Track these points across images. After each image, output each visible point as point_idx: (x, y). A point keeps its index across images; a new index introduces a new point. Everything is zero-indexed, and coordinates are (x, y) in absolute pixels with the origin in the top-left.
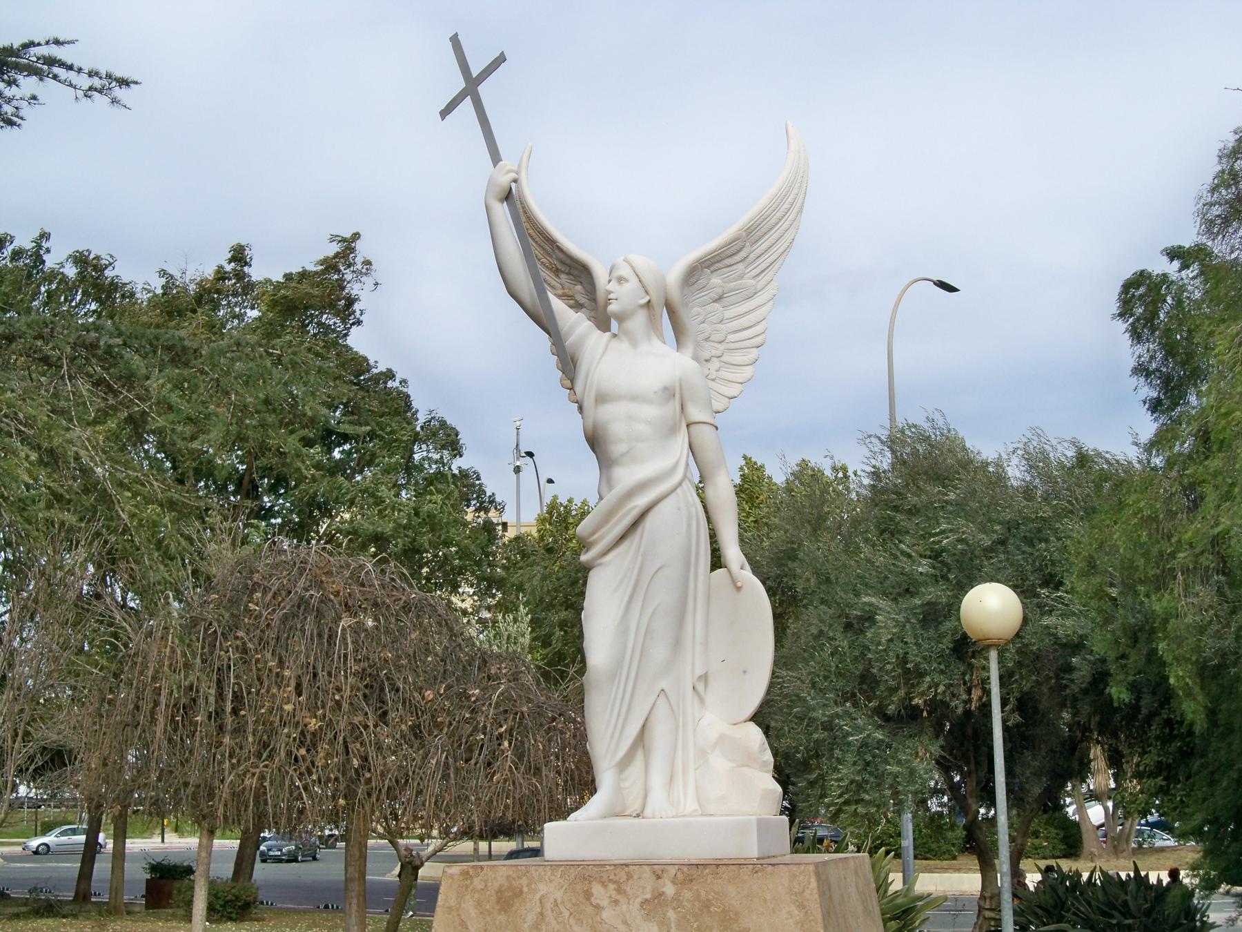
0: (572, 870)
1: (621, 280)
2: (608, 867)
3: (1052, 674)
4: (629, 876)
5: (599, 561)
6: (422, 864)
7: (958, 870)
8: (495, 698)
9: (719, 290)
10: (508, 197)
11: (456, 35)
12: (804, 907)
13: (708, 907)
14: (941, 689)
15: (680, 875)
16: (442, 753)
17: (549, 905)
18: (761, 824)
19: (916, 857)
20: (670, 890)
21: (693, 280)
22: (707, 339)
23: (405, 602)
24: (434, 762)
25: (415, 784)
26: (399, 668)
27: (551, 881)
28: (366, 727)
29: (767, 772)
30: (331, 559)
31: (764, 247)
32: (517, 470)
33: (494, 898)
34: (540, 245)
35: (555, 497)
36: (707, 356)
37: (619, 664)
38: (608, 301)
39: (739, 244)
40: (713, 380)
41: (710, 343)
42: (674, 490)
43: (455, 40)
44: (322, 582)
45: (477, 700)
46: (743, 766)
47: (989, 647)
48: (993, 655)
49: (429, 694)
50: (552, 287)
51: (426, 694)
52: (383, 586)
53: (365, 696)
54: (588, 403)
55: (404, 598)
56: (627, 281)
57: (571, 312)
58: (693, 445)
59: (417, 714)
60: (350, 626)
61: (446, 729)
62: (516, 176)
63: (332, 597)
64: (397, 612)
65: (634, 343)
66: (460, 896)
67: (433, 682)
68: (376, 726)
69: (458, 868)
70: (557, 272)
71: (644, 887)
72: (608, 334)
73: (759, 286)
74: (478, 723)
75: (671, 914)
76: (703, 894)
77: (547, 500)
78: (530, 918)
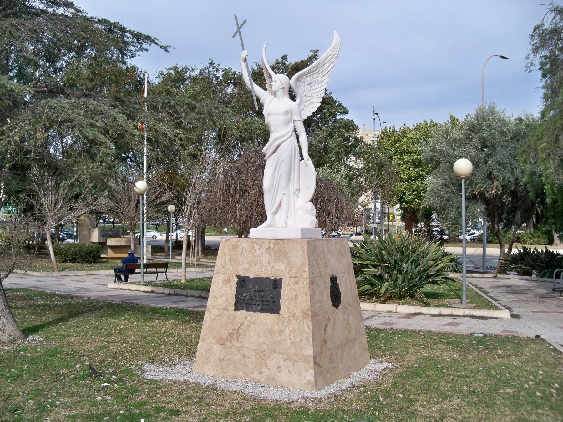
3: (522, 185)
9: (309, 82)
14: (483, 189)
15: (275, 243)
17: (244, 249)
20: (272, 246)
32: (374, 119)
35: (386, 127)
36: (305, 101)
43: (236, 16)
47: (463, 178)
48: (463, 181)
65: (279, 99)
66: (224, 247)
73: (323, 80)
75: (272, 252)
77: (383, 128)
78: (240, 252)
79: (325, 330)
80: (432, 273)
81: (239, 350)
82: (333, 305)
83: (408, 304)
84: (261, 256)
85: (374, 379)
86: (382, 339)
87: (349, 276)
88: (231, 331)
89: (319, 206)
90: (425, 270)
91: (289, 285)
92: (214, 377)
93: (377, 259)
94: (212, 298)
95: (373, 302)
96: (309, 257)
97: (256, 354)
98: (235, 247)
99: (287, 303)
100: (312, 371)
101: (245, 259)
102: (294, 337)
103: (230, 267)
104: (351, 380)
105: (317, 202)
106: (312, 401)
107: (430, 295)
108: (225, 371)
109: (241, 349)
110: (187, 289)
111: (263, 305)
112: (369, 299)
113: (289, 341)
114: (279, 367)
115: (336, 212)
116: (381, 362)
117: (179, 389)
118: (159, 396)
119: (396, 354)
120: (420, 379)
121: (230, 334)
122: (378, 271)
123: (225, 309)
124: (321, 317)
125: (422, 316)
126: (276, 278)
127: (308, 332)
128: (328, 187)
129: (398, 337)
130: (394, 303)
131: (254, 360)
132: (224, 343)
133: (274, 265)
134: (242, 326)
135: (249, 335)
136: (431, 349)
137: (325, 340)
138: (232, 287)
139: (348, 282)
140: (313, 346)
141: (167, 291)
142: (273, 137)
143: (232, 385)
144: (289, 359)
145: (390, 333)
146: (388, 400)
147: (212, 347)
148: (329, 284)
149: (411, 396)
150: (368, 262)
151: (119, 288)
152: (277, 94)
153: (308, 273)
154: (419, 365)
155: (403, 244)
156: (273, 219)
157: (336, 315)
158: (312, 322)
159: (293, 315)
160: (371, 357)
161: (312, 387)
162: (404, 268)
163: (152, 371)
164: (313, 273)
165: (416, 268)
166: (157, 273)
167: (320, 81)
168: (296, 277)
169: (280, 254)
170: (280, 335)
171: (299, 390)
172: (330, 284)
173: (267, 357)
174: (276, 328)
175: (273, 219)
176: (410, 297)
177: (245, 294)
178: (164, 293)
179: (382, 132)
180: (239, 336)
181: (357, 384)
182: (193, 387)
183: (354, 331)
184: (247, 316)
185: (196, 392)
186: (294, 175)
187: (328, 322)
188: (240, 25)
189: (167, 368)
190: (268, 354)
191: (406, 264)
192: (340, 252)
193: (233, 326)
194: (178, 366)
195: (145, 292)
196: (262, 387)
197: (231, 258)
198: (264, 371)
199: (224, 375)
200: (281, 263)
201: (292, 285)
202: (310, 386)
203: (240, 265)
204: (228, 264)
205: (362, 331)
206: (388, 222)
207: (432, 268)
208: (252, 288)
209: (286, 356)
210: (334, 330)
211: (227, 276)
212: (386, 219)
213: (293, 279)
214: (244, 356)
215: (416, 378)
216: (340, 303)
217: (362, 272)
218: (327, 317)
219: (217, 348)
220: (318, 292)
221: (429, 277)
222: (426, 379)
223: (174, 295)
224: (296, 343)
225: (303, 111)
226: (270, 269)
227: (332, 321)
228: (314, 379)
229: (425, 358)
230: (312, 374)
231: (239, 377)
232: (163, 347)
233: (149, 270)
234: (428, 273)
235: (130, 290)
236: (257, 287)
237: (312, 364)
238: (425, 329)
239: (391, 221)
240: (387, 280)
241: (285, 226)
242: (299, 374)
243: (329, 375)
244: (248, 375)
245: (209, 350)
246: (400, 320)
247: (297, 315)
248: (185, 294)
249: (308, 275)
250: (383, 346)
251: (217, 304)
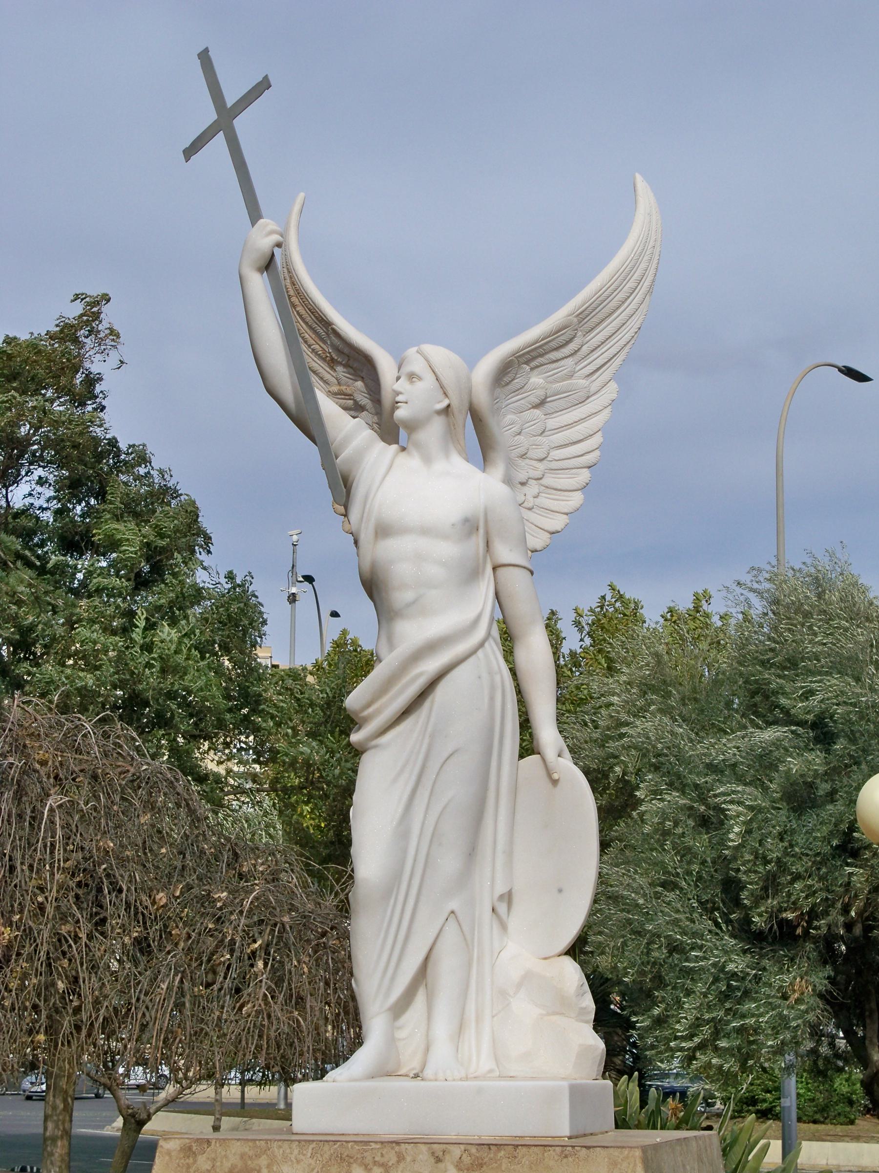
0: (326, 1148)
1: (412, 377)
2: (373, 1146)
4: (401, 1158)
5: (374, 743)
6: (149, 1118)
7: (857, 1138)
8: (247, 904)
9: (541, 393)
10: (268, 265)
11: (206, 50)
15: (467, 1159)
16: (176, 975)
18: (577, 1094)
19: (799, 1120)
21: (506, 379)
22: (523, 456)
23: (133, 775)
24: (164, 986)
25: (140, 1015)
26: (123, 862)
27: (298, 1162)
28: (76, 939)
29: (587, 1022)
30: (39, 717)
31: (600, 338)
32: (293, 598)
34: (310, 327)
36: (522, 476)
38: (395, 405)
39: (567, 334)
40: (530, 509)
41: (527, 461)
42: (473, 652)
44: (25, 746)
45: (225, 905)
46: (555, 1013)
49: (162, 897)
50: (326, 382)
51: (158, 897)
52: (106, 755)
53: (77, 897)
54: (366, 536)
55: (132, 770)
56: (420, 379)
57: (345, 417)
58: (501, 594)
59: (145, 923)
60: (60, 806)
61: (182, 944)
63: (37, 766)
64: (123, 789)
65: (427, 460)
67: (167, 880)
68: (90, 937)
69: (177, 1141)
70: (332, 363)
72: (394, 447)
73: (593, 388)
74: (224, 936)
167: (582, 394)
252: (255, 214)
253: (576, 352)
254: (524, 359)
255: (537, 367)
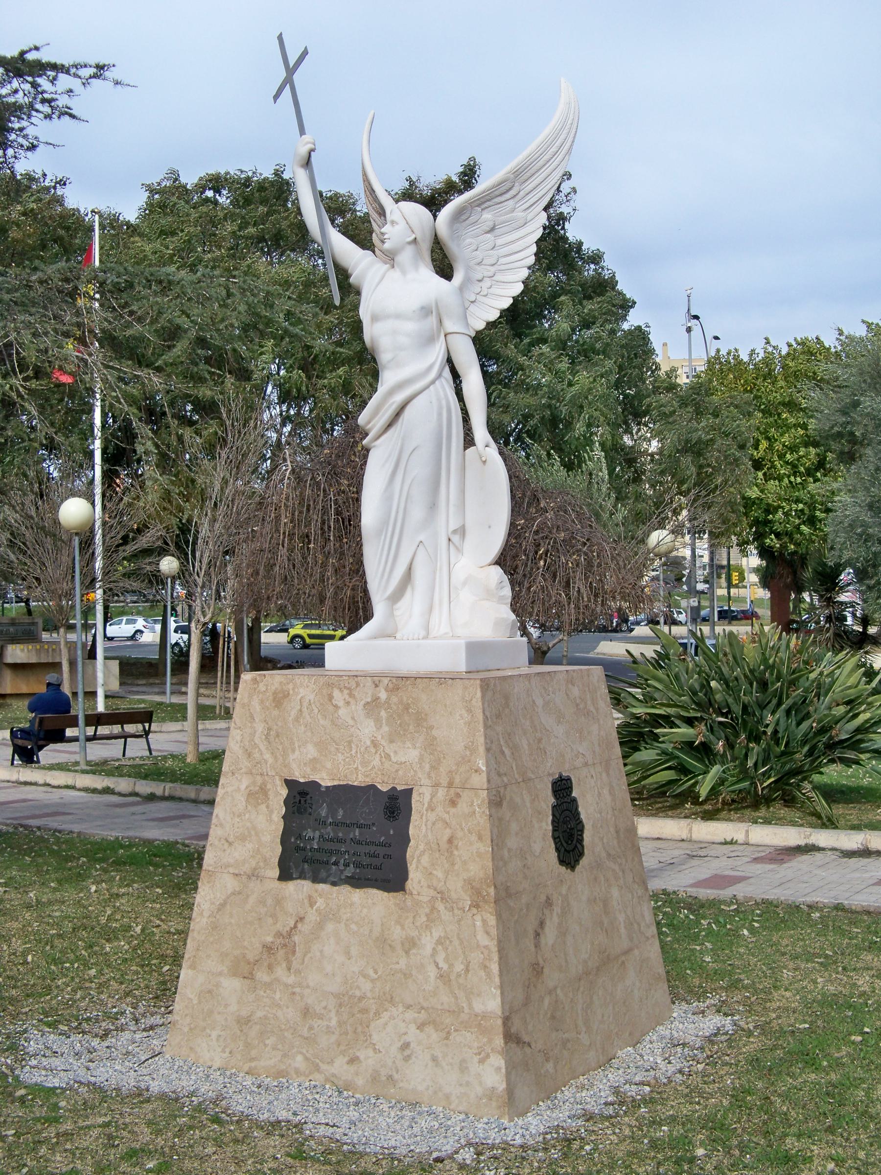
5: (373, 444)
9: (491, 224)
11: (281, 34)
12: (471, 712)
13: (407, 709)
15: (391, 686)
17: (305, 704)
20: (383, 695)
21: (463, 217)
22: (479, 264)
29: (506, 604)
32: (689, 330)
33: (271, 698)
37: (385, 523)
40: (485, 296)
42: (427, 387)
43: (280, 38)
48: (169, 580)
56: (397, 224)
62: (313, 146)
65: (404, 273)
66: (250, 696)
71: (366, 693)
73: (529, 218)
75: (383, 714)
76: (405, 699)
78: (293, 713)
79: (537, 934)
80: (844, 736)
81: (294, 993)
82: (562, 862)
83: (781, 821)
84: (351, 722)
85: (680, 1071)
86: (706, 936)
87: (608, 774)
88: (269, 939)
89: (542, 563)
90: (823, 731)
91: (431, 808)
92: (222, 1070)
93: (694, 702)
94: (217, 843)
95: (685, 817)
96: (486, 727)
97: (340, 1005)
98: (280, 699)
99: (425, 860)
100: (498, 1061)
101: (309, 734)
102: (446, 960)
103: (267, 756)
104: (614, 1077)
105: (536, 553)
106: (495, 1158)
107: (833, 794)
108: (254, 1053)
109: (297, 990)
110: (197, 783)
111: (358, 865)
112: (673, 807)
113: (432, 972)
114: (406, 1046)
115: (586, 578)
116: (703, 1012)
117: (107, 1125)
118: (43, 1151)
119: (746, 988)
120: (813, 1076)
121: (268, 949)
122: (697, 734)
123: (254, 875)
124: (524, 899)
125: (818, 855)
126: (394, 789)
127: (486, 947)
128: (566, 512)
129: (752, 930)
130: (741, 820)
131: (334, 1022)
132: (251, 973)
133: (390, 749)
134: (299, 925)
135: (321, 951)
136: (844, 969)
137: (538, 964)
138: (271, 812)
139: (606, 791)
140: (502, 987)
141: (145, 787)
142: (388, 379)
143: (271, 1098)
144: (434, 1023)
145: (730, 916)
146: (719, 1155)
147: (218, 985)
148: (548, 800)
149: (788, 1140)
150: (671, 711)
151: (22, 779)
152: (399, 258)
153: (484, 775)
154: (811, 1023)
155: (765, 660)
156: (391, 615)
157: (569, 888)
158: (499, 916)
159: (443, 896)
160: (675, 998)
161: (499, 1107)
162: (767, 726)
163: (48, 1053)
164: (499, 775)
165: (799, 724)
166: (125, 737)
167: (522, 222)
168: (450, 785)
169: (406, 718)
170: (407, 952)
171: (462, 1116)
172: (552, 800)
173: (372, 1014)
174: (397, 933)
175: (391, 615)
176: (785, 801)
177: (309, 833)
178: (136, 794)
179: (709, 361)
180: (294, 952)
181: (632, 1091)
182: (153, 1111)
183: (623, 930)
184: (315, 895)
185: (158, 1132)
186: (450, 489)
187: (546, 912)
188: (291, 64)
189: (95, 1042)
190: (374, 1007)
191: (773, 713)
192: (581, 706)
193: (275, 924)
194: (127, 1035)
195: (86, 790)
196: (357, 1104)
197: (269, 729)
198: (362, 1057)
199: (253, 1064)
200: (408, 744)
201: (440, 809)
202: (494, 1104)
203: (293, 751)
204: (263, 748)
205: (648, 927)
206: (729, 588)
207: (841, 723)
208: (327, 817)
209: (423, 1015)
210: (563, 932)
211: (259, 780)
212: (723, 581)
213: (441, 793)
214: (306, 1012)
215: (802, 1070)
216: (581, 854)
217: (656, 737)
218: (543, 898)
219: (231, 986)
220: (514, 827)
221: (831, 746)
222: (833, 1076)
223: (163, 798)
224: (453, 977)
225: (472, 308)
226: (376, 762)
227: (557, 909)
228: (504, 1085)
229: (830, 1002)
230: (499, 1069)
231: (292, 1073)
232: (93, 972)
233: (103, 730)
234: (831, 738)
235: (49, 785)
236: (341, 812)
237: (499, 1041)
238: (824, 898)
239: (737, 586)
240: (724, 755)
241: (423, 633)
242: (463, 1067)
243: (550, 1066)
244: (317, 1069)
245: (209, 993)
246: (759, 868)
247: (454, 896)
248: (192, 795)
249: (485, 780)
250: (708, 959)
251: (232, 861)
252: (302, 132)
253: (515, 196)
254: (475, 204)
255: (487, 208)
